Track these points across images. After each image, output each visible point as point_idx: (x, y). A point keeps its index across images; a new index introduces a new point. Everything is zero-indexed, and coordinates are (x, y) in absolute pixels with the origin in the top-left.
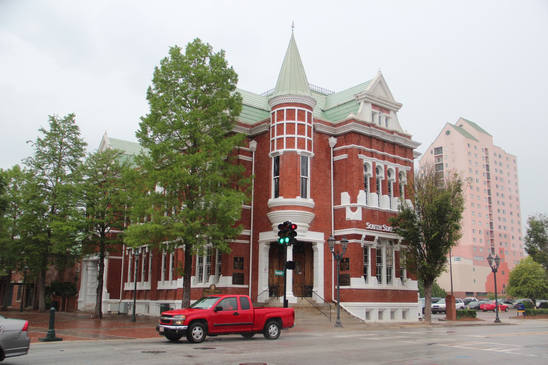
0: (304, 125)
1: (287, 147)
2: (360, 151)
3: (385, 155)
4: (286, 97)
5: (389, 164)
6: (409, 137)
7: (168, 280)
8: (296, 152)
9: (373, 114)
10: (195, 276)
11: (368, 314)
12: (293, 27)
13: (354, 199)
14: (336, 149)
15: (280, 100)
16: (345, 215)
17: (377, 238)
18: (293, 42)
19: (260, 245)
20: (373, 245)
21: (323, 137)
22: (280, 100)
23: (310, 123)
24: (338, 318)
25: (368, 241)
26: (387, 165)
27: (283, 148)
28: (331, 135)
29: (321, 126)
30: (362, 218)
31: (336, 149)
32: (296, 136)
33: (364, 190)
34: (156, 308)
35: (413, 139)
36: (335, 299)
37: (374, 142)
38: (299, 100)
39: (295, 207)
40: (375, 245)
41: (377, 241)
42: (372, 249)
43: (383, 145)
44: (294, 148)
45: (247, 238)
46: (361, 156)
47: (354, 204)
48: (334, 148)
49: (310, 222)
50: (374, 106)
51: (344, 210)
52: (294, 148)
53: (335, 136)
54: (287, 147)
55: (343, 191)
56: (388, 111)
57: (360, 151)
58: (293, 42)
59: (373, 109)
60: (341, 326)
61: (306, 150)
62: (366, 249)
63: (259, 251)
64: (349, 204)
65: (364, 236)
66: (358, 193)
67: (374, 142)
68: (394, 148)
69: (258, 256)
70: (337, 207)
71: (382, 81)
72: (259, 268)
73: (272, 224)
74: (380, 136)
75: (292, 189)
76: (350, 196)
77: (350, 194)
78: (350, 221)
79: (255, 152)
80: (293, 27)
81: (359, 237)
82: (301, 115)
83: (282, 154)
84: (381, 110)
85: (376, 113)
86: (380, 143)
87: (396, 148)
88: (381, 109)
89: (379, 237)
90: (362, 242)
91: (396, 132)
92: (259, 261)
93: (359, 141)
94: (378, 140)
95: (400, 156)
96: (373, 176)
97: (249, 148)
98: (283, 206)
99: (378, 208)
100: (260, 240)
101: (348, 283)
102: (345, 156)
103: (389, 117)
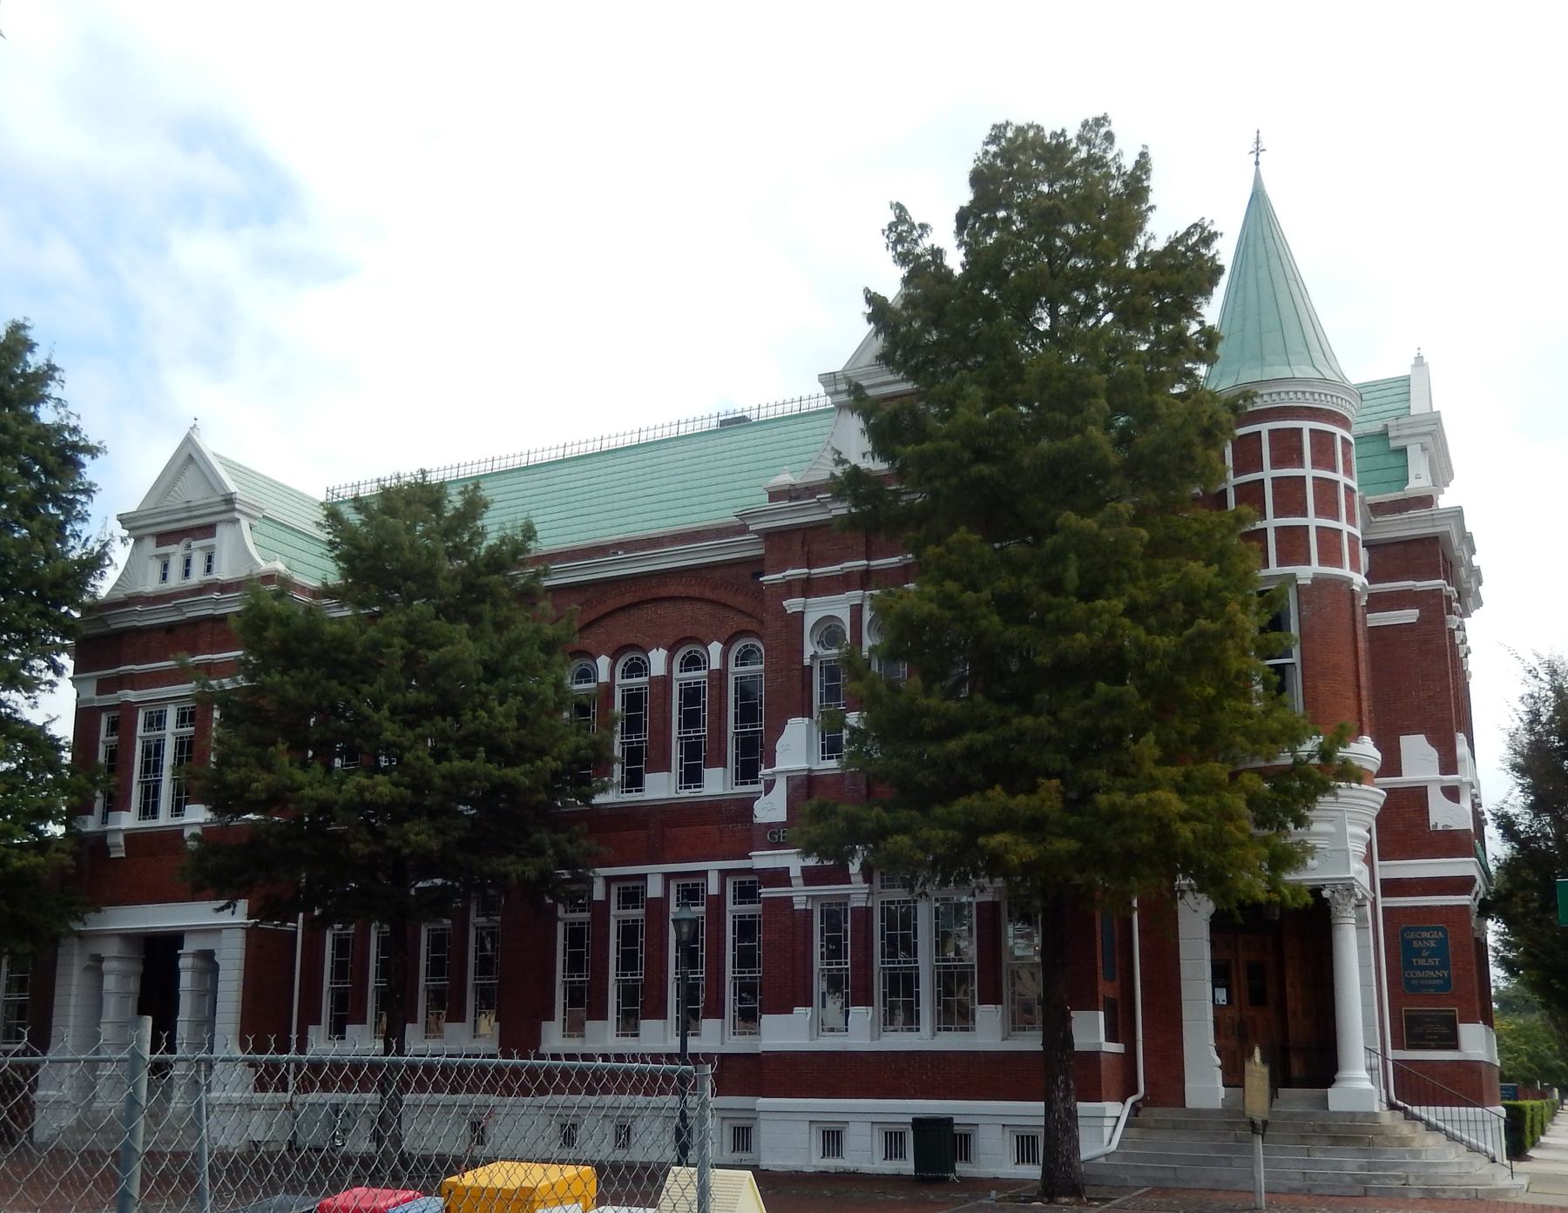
4: (1313, 386)
7: (606, 1018)
27: (1308, 562)
47: (1449, 779)
51: (1418, 796)
92: (1182, 956)
101: (1452, 1042)
102: (1410, 615)
103: (212, 547)
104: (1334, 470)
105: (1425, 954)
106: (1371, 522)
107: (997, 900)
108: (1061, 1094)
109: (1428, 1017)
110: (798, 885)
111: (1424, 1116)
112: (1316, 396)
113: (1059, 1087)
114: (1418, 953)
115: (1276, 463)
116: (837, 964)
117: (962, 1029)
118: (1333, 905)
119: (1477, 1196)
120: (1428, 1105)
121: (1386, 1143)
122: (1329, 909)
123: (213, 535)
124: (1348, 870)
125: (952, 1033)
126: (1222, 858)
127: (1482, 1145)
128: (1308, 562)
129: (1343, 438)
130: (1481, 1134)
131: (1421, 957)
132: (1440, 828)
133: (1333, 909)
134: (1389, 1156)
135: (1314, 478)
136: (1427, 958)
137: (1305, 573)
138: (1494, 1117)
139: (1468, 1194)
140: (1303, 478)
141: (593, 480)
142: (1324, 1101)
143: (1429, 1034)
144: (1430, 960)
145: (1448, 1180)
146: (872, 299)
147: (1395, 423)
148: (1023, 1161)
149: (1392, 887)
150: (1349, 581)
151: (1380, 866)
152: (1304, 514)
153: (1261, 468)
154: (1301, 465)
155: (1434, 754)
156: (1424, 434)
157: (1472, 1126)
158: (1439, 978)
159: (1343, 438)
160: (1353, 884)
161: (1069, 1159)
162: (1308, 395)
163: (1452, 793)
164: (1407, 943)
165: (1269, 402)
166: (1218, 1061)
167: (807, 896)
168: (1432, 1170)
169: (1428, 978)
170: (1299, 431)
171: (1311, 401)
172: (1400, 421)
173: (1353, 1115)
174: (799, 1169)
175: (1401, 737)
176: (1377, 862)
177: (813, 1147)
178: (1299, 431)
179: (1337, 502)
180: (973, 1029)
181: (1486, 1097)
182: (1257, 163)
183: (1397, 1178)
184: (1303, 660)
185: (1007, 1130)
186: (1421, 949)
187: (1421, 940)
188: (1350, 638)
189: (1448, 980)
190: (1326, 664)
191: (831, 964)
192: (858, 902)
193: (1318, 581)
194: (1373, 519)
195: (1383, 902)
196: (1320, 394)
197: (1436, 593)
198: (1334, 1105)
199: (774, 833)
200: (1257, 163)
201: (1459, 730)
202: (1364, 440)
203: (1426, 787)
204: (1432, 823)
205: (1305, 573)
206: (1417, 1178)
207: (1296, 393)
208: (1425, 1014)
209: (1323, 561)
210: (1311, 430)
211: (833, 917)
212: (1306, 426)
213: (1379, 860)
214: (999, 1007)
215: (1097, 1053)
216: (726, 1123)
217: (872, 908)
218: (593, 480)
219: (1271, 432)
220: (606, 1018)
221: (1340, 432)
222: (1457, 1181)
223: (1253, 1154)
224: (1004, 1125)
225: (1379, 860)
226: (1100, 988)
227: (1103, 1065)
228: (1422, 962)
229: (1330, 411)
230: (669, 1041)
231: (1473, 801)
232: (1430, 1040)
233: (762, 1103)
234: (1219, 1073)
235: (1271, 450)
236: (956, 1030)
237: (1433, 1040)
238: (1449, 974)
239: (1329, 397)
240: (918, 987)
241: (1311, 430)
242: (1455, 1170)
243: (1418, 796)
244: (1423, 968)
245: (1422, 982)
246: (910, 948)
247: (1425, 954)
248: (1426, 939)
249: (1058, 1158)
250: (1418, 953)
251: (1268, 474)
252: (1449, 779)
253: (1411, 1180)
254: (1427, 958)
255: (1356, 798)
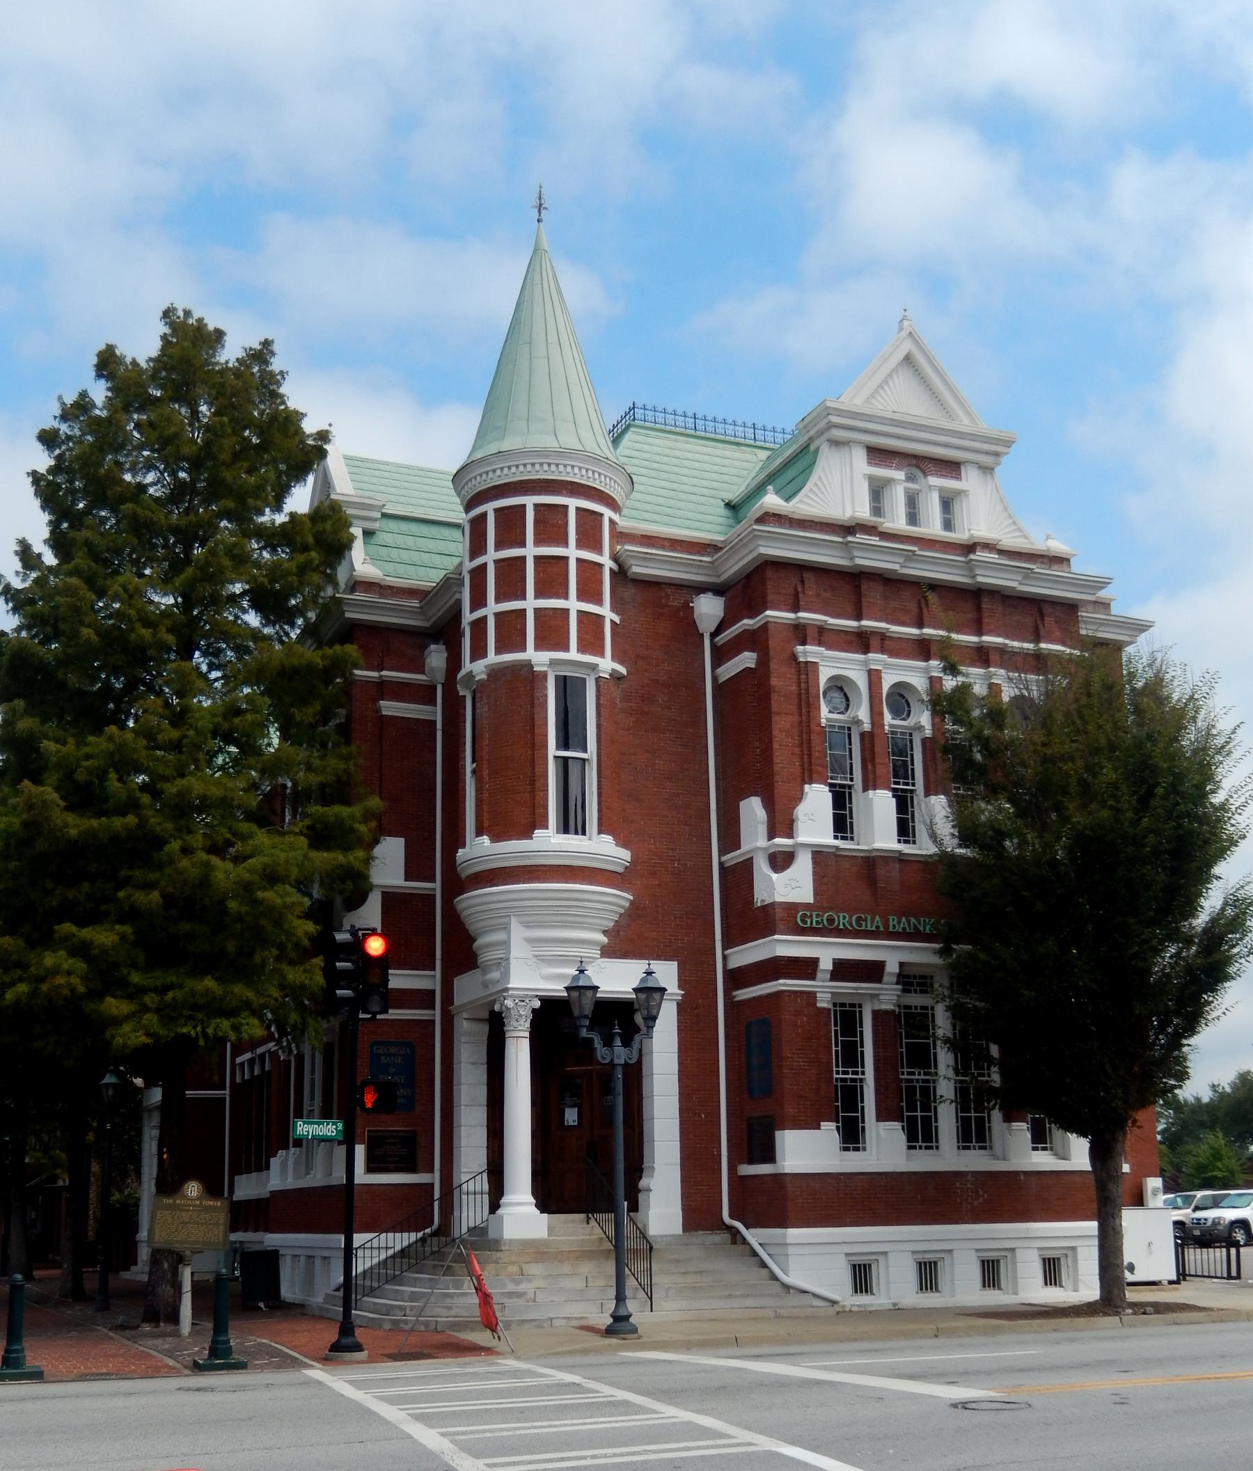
0: (566, 559)
2: (801, 633)
3: (866, 632)
4: (492, 464)
5: (886, 665)
6: (1060, 560)
8: (528, 665)
9: (878, 491)
11: (862, 1277)
12: (540, 207)
13: (781, 823)
14: (722, 639)
15: (487, 473)
17: (892, 968)
20: (877, 995)
21: (668, 596)
22: (487, 473)
23: (597, 547)
24: (318, 1445)
25: (854, 981)
26: (879, 671)
28: (701, 589)
29: (646, 558)
30: (816, 894)
31: (722, 639)
32: (573, 604)
33: (825, 783)
35: (1079, 567)
36: (731, 1216)
37: (872, 593)
38: (537, 467)
39: (530, 872)
40: (887, 996)
41: (895, 979)
42: (876, 1014)
43: (922, 603)
44: (524, 649)
45: (423, 998)
46: (809, 652)
48: (714, 635)
49: (611, 924)
50: (878, 454)
51: (746, 867)
52: (524, 649)
53: (718, 590)
56: (951, 467)
57: (801, 633)
59: (876, 465)
61: (573, 654)
62: (848, 1017)
64: (762, 842)
65: (826, 965)
66: (799, 797)
67: (872, 593)
68: (979, 608)
70: (732, 858)
71: (918, 356)
73: (475, 940)
74: (896, 567)
78: (768, 909)
79: (443, 684)
80: (540, 207)
81: (807, 968)
82: (590, 532)
83: (484, 676)
84: (918, 467)
85: (889, 482)
86: (906, 595)
87: (984, 606)
88: (914, 462)
89: (901, 964)
90: (824, 991)
91: (988, 546)
93: (796, 595)
94: (891, 582)
95: (1007, 637)
96: (873, 723)
97: (423, 672)
99: (899, 852)
101: (768, 1155)
102: (747, 659)
103: (959, 493)
105: (392, 1070)
116: (925, 1074)
117: (927, 1148)
119: (436, 1329)
123: (958, 476)
125: (972, 1152)
131: (389, 1075)
135: (578, 560)
140: (566, 559)
141: (653, 473)
152: (566, 596)
153: (522, 544)
171: (598, 482)
180: (864, 1149)
191: (846, 1073)
193: (496, 673)
195: (434, 1015)
199: (805, 915)
209: (582, 649)
210: (578, 509)
218: (653, 473)
219: (497, 511)
221: (607, 513)
236: (921, 1148)
239: (603, 477)
240: (862, 1101)
241: (578, 509)
251: (530, 551)
255: (517, 900)
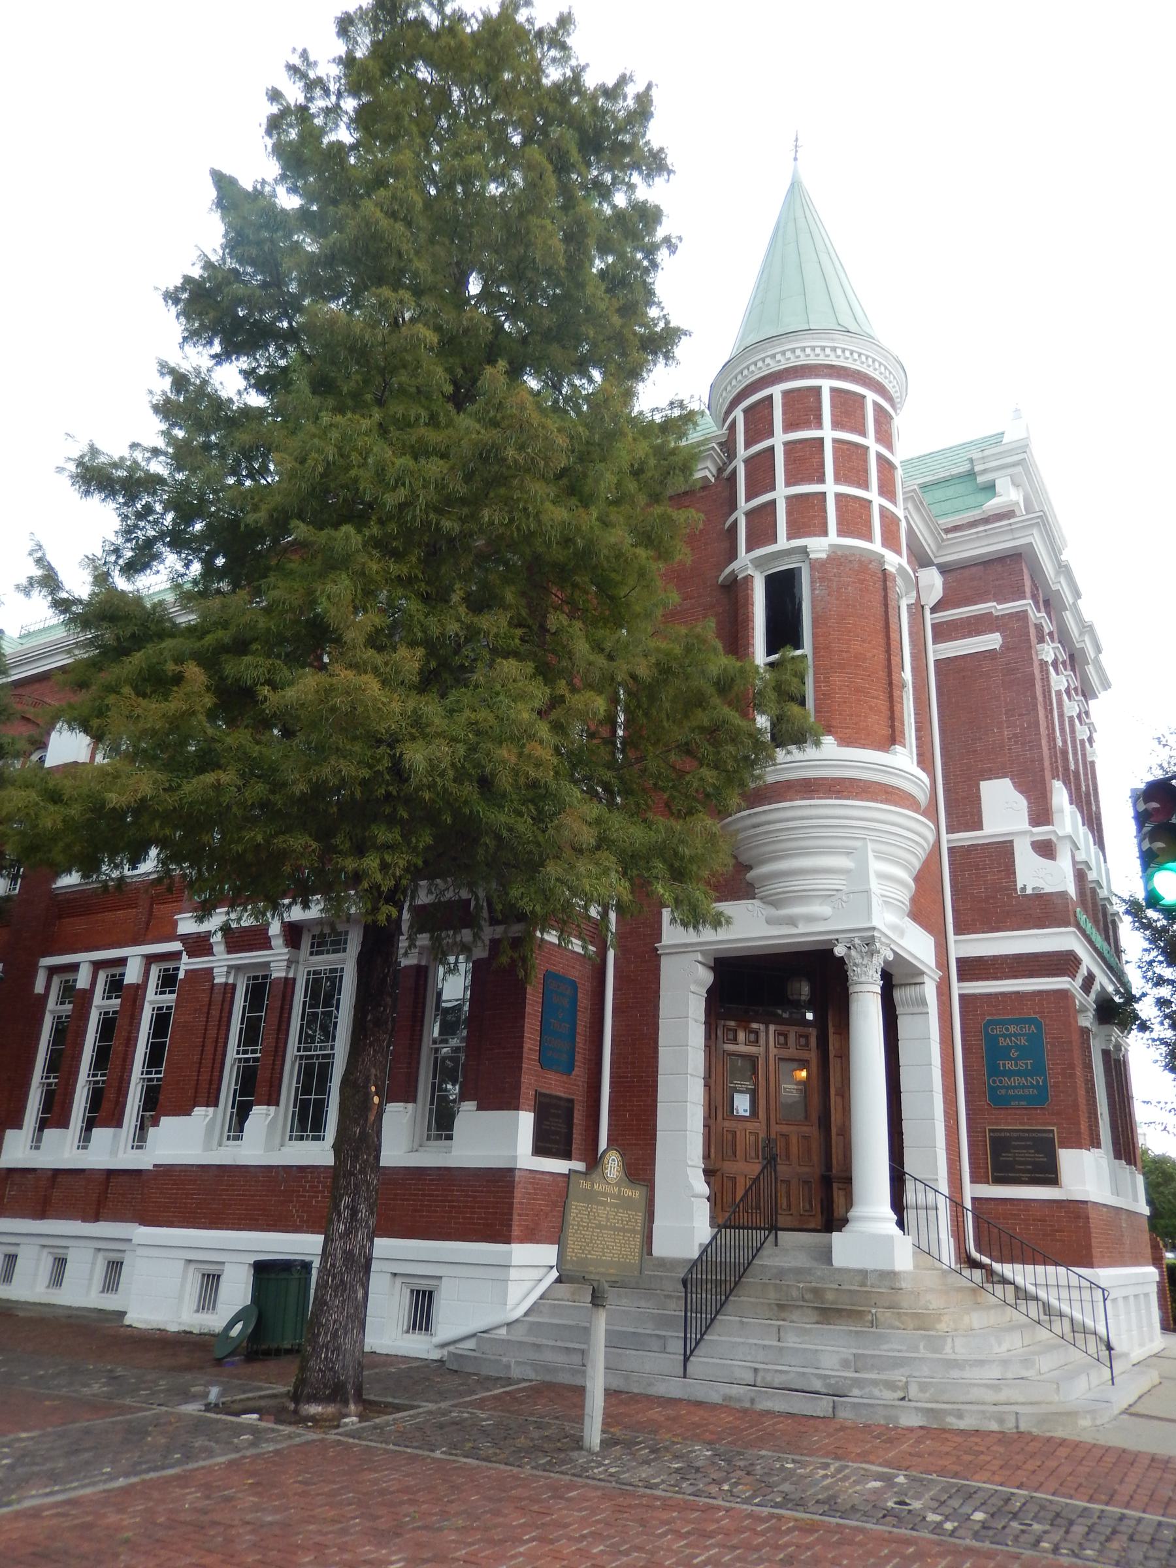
1: (841, 533)
7: (119, 1125)
10: (277, 1104)
16: (1012, 873)
18: (795, 189)
19: (666, 964)
27: (825, 533)
34: (94, 1264)
47: (1041, 832)
48: (934, 610)
51: (1003, 852)
54: (841, 533)
55: (992, 774)
58: (795, 189)
60: (103, 1291)
63: (662, 993)
64: (1024, 825)
69: (656, 1016)
70: (966, 838)
72: (660, 1078)
75: (871, 708)
76: (1028, 798)
77: (1021, 787)
92: (661, 1042)
98: (833, 779)
100: (663, 943)
101: (1048, 1174)
102: (992, 641)
104: (863, 433)
106: (943, 540)
107: (423, 963)
108: (342, 1227)
109: (1018, 1139)
110: (221, 954)
111: (1019, 1280)
112: (839, 352)
113: (339, 1214)
114: (1005, 1053)
115: (789, 426)
118: (850, 965)
120: (1024, 1262)
121: (897, 1324)
122: (845, 978)
124: (869, 916)
126: (538, 832)
127: (1089, 1323)
128: (825, 533)
129: (875, 404)
130: (1087, 1306)
131: (1011, 1059)
132: (1029, 891)
133: (850, 973)
134: (895, 1344)
136: (1015, 1059)
137: (819, 546)
138: (1084, 1283)
139: (1001, 1421)
142: (826, 1255)
143: (1021, 1163)
144: (1020, 1063)
145: (976, 1394)
146: (223, 183)
147: (980, 455)
148: (414, 1328)
149: (971, 968)
150: (881, 559)
151: (956, 941)
152: (821, 480)
154: (819, 425)
155: (1021, 804)
156: (1014, 465)
157: (1075, 1294)
158: (1032, 1086)
159: (875, 404)
160: (873, 937)
161: (335, 1335)
162: (828, 351)
163: (1045, 849)
164: (992, 1041)
165: (783, 361)
166: (704, 1189)
167: (230, 967)
168: (955, 1373)
169: (1019, 1087)
170: (817, 391)
172: (986, 453)
173: (864, 1273)
174: (162, 1327)
175: (982, 783)
176: (951, 937)
177: (187, 1296)
178: (817, 391)
179: (866, 471)
181: (1096, 1252)
182: (795, 159)
183: (891, 1385)
184: (816, 649)
185: (399, 1281)
186: (1009, 1048)
187: (1010, 1036)
188: (880, 625)
189: (1042, 1089)
190: (845, 655)
192: (278, 973)
193: (837, 558)
194: (945, 537)
196: (844, 350)
197: (1022, 616)
198: (840, 1259)
200: (795, 159)
201: (1055, 776)
202: (952, 482)
203: (1012, 842)
204: (1019, 885)
205: (819, 546)
206: (923, 1387)
207: (813, 348)
208: (1015, 1135)
211: (259, 989)
212: (826, 385)
213: (955, 934)
214: (410, 1106)
215: (511, 1171)
216: (101, 1256)
217: (294, 980)
220: (119, 1125)
222: (990, 1396)
223: (587, 1341)
224: (395, 1274)
225: (955, 934)
226: (526, 1079)
227: (519, 1194)
228: (1010, 1065)
229: (859, 372)
230: (121, 1155)
231: (1073, 857)
232: (1020, 1171)
233: (142, 1233)
234: (706, 1206)
235: (784, 413)
237: (1028, 1171)
238: (1045, 1081)
242: (994, 1372)
243: (1003, 852)
244: (1011, 1074)
245: (1011, 1092)
246: (329, 1034)
247: (1014, 1054)
248: (1015, 1035)
249: (319, 1334)
250: (1005, 1053)
252: (1041, 832)
253: (913, 1391)
254: (1015, 1059)
